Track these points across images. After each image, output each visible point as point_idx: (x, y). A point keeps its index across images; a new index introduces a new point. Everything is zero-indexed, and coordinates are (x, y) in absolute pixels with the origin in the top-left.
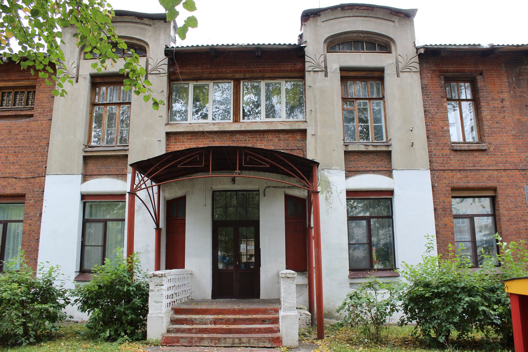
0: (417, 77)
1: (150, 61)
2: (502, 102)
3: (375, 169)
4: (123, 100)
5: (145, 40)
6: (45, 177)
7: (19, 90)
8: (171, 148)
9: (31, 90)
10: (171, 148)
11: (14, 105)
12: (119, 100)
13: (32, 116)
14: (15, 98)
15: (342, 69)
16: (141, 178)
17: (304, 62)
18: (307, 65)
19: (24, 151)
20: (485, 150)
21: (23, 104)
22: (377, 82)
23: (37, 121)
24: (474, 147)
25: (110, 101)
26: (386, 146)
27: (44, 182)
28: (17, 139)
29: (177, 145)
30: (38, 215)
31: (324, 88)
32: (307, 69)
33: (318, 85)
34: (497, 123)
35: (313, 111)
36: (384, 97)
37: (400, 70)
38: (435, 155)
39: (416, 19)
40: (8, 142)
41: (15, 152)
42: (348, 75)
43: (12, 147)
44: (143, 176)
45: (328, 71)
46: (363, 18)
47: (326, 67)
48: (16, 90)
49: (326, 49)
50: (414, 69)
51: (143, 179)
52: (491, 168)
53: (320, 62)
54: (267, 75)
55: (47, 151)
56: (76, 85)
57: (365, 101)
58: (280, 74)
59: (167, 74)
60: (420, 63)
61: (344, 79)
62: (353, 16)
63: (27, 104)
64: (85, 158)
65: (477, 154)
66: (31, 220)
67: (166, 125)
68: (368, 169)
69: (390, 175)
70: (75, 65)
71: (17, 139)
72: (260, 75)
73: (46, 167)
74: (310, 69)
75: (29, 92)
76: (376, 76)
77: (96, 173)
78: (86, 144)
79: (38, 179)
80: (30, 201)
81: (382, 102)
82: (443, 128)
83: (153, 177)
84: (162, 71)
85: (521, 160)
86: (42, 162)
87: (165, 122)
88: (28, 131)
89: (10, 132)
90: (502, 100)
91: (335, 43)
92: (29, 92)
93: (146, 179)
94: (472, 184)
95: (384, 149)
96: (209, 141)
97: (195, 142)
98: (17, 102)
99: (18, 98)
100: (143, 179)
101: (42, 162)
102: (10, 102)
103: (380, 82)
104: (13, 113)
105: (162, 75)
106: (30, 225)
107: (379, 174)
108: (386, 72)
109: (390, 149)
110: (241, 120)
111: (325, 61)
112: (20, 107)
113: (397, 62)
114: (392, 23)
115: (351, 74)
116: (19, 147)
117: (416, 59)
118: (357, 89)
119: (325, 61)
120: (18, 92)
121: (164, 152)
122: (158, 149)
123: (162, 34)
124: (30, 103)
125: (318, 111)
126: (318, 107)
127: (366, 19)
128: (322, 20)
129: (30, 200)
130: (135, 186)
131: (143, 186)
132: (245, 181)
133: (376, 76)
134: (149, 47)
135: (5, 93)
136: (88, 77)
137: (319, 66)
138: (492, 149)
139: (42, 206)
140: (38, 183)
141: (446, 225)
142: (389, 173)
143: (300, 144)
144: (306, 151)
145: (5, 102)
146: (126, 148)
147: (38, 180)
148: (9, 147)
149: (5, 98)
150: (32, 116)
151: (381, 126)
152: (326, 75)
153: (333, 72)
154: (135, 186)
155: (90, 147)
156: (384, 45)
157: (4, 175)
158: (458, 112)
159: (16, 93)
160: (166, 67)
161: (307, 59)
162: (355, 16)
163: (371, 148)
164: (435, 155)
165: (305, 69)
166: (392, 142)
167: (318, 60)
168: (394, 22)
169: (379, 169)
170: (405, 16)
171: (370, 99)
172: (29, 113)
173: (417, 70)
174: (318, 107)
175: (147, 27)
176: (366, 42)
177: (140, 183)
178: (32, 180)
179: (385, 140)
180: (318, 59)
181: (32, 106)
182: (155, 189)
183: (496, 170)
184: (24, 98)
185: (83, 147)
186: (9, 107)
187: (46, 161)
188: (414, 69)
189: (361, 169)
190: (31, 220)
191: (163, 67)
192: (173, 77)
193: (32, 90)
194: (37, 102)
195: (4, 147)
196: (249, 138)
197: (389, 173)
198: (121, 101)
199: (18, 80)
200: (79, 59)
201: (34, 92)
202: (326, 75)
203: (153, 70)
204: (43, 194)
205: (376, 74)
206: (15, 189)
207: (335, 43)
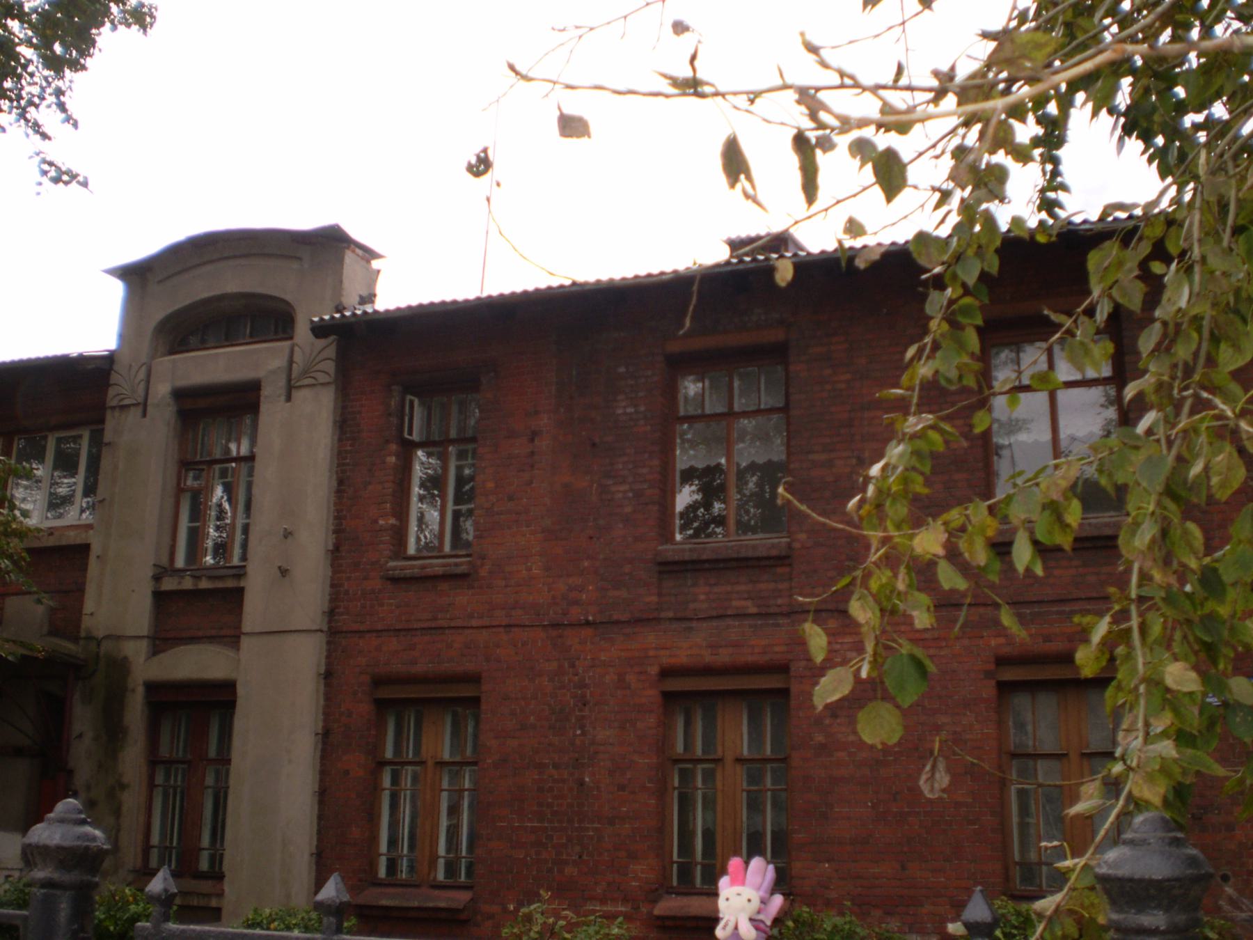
2: (532, 440)
3: (214, 632)
18: (112, 392)
20: (463, 576)
24: (436, 566)
31: (144, 441)
34: (511, 499)
38: (347, 592)
45: (149, 402)
50: (322, 378)
52: (474, 623)
53: (137, 381)
65: (444, 586)
68: (200, 634)
74: (114, 403)
82: (376, 521)
85: (554, 598)
90: (534, 436)
94: (420, 668)
95: (230, 584)
108: (266, 392)
114: (295, 265)
132: (417, 760)
138: (483, 572)
141: (347, 772)
142: (233, 638)
152: (144, 414)
156: (270, 319)
158: (1063, 435)
164: (347, 592)
165: (104, 403)
166: (253, 568)
168: (300, 259)
183: (487, 627)
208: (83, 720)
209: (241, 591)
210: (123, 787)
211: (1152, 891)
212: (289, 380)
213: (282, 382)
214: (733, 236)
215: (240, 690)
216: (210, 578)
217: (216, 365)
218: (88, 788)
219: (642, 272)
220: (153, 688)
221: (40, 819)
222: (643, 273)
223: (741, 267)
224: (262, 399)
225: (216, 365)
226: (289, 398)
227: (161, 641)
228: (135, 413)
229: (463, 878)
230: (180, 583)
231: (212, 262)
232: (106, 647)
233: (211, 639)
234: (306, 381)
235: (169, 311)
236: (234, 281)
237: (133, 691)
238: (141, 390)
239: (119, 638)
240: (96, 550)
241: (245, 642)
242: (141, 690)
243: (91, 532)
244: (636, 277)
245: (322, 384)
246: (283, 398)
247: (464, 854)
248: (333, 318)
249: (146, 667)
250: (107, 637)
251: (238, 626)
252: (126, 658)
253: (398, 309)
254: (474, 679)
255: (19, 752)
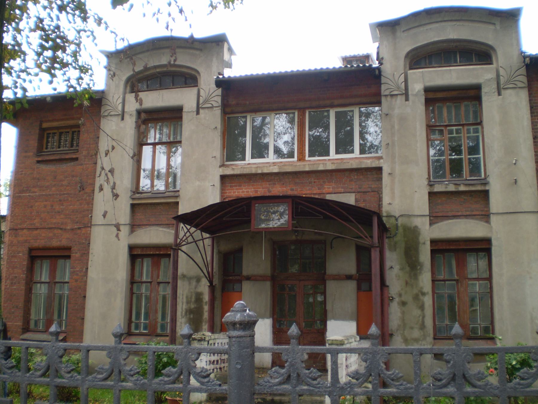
0: (524, 95)
1: (202, 93)
3: (468, 213)
4: (174, 138)
5: (198, 69)
6: (90, 227)
7: (64, 130)
8: (226, 193)
9: (75, 131)
10: (226, 193)
11: (59, 147)
12: (169, 138)
13: (76, 159)
14: (60, 139)
15: (427, 90)
16: (186, 230)
17: (379, 84)
18: (383, 87)
19: (70, 199)
21: (67, 145)
22: (473, 103)
23: (81, 165)
25: (160, 140)
26: (482, 184)
27: (90, 234)
28: (62, 186)
29: (233, 189)
30: (84, 270)
32: (383, 93)
33: (397, 111)
35: (390, 144)
36: (481, 122)
37: (502, 86)
39: (524, 23)
40: (54, 189)
41: (60, 201)
42: (435, 97)
43: (57, 195)
44: (189, 227)
45: (410, 93)
46: (455, 23)
47: (406, 88)
48: (61, 131)
49: (408, 66)
50: (520, 85)
51: (188, 231)
54: (336, 102)
55: (93, 199)
56: (122, 124)
57: (459, 127)
58: (353, 100)
59: (220, 108)
60: (529, 76)
61: (428, 102)
62: (441, 21)
63: (72, 146)
64: (133, 206)
66: (77, 275)
67: (220, 167)
68: (460, 214)
69: (488, 221)
70: (120, 100)
71: (62, 186)
72: (328, 102)
73: (91, 217)
74: (387, 93)
75: (73, 132)
76: (471, 94)
77: (145, 223)
78: (134, 190)
79: (84, 230)
80: (76, 254)
81: (479, 127)
83: (202, 227)
84: (215, 104)
86: (88, 210)
87: (219, 164)
88: (73, 176)
89: (55, 178)
91: (419, 58)
92: (73, 132)
93: (193, 229)
95: (479, 188)
96: (269, 185)
97: (253, 185)
98: (62, 143)
99: (63, 139)
100: (188, 231)
101: (88, 210)
102: (55, 144)
103: (477, 103)
104: (57, 157)
105: (215, 109)
106: (76, 281)
107: (473, 219)
108: (484, 90)
109: (487, 188)
110: (307, 158)
111: (406, 81)
112: (65, 149)
113: (498, 76)
114: (492, 27)
115: (440, 95)
116: (64, 194)
117: (523, 71)
118: (447, 114)
119: (406, 81)
120: (63, 133)
121: (218, 200)
122: (212, 197)
123: (214, 59)
124: (75, 145)
125: (396, 144)
126: (396, 139)
127: (458, 23)
128: (402, 30)
129: (76, 253)
130: (179, 240)
131: (190, 239)
133: (471, 94)
134: (200, 75)
135: (50, 134)
136: (135, 113)
137: (399, 88)
139: (88, 260)
140: (84, 234)
142: (486, 217)
143: (374, 185)
144: (382, 194)
145: (49, 144)
146: (177, 194)
147: (83, 231)
148: (54, 195)
149: (50, 140)
150: (76, 159)
151: (479, 158)
152: (407, 99)
153: (416, 95)
154: (179, 240)
155: (138, 193)
156: (482, 54)
157: (50, 226)
159: (61, 134)
160: (219, 99)
161: (383, 80)
162: (445, 21)
163: (462, 188)
166: (491, 180)
167: (396, 80)
168: (494, 24)
169: (474, 213)
170: (511, 17)
171: (463, 125)
172: (74, 156)
173: (523, 85)
174: (396, 139)
175: (198, 52)
176: (460, 52)
177: (185, 235)
178: (79, 231)
179: (483, 176)
180: (396, 78)
181: (77, 148)
182: (208, 242)
184: (69, 139)
185: (130, 194)
186: (54, 150)
187: (92, 210)
188: (520, 85)
189: (450, 214)
190: (77, 275)
191: (216, 99)
192: (228, 110)
193: (76, 130)
194: (81, 143)
195: (50, 195)
196: (315, 179)
197: (486, 217)
198: (172, 140)
199: (62, 120)
200: (125, 93)
201: (79, 131)
202: (407, 99)
203: (205, 102)
204: (89, 246)
205: (472, 93)
206: (61, 241)
207: (419, 58)
208: (393, 260)
209: (177, 203)
210: (424, 294)
211: (374, 329)
212: (498, 84)
213: (495, 86)
214: (348, 55)
215: (494, 242)
216: (466, 185)
217: (155, 99)
218: (400, 295)
219: (283, 71)
220: (433, 242)
221: (228, 311)
222: (295, 70)
223: (346, 69)
224: (483, 94)
225: (155, 99)
226: (499, 94)
227: (435, 218)
228: (400, 100)
229: (41, 328)
230: (446, 188)
231: (437, 22)
232: (400, 221)
233: (466, 216)
234: (511, 86)
235: (413, 47)
236: (163, 59)
237: (424, 243)
238: (120, 107)
239: (409, 216)
240: (386, 170)
241: (493, 218)
242: (428, 243)
243: (382, 161)
244: (246, 75)
245: (520, 88)
246: (496, 94)
247: (64, 318)
248: (358, 66)
249: (429, 232)
250: (401, 216)
251: (489, 210)
252: (416, 227)
253: (235, 77)
254: (69, 249)
255: (349, 277)
